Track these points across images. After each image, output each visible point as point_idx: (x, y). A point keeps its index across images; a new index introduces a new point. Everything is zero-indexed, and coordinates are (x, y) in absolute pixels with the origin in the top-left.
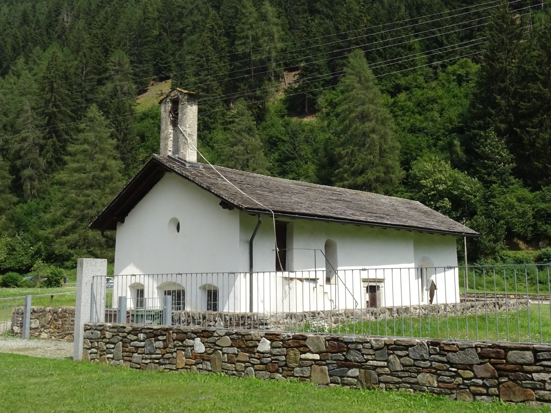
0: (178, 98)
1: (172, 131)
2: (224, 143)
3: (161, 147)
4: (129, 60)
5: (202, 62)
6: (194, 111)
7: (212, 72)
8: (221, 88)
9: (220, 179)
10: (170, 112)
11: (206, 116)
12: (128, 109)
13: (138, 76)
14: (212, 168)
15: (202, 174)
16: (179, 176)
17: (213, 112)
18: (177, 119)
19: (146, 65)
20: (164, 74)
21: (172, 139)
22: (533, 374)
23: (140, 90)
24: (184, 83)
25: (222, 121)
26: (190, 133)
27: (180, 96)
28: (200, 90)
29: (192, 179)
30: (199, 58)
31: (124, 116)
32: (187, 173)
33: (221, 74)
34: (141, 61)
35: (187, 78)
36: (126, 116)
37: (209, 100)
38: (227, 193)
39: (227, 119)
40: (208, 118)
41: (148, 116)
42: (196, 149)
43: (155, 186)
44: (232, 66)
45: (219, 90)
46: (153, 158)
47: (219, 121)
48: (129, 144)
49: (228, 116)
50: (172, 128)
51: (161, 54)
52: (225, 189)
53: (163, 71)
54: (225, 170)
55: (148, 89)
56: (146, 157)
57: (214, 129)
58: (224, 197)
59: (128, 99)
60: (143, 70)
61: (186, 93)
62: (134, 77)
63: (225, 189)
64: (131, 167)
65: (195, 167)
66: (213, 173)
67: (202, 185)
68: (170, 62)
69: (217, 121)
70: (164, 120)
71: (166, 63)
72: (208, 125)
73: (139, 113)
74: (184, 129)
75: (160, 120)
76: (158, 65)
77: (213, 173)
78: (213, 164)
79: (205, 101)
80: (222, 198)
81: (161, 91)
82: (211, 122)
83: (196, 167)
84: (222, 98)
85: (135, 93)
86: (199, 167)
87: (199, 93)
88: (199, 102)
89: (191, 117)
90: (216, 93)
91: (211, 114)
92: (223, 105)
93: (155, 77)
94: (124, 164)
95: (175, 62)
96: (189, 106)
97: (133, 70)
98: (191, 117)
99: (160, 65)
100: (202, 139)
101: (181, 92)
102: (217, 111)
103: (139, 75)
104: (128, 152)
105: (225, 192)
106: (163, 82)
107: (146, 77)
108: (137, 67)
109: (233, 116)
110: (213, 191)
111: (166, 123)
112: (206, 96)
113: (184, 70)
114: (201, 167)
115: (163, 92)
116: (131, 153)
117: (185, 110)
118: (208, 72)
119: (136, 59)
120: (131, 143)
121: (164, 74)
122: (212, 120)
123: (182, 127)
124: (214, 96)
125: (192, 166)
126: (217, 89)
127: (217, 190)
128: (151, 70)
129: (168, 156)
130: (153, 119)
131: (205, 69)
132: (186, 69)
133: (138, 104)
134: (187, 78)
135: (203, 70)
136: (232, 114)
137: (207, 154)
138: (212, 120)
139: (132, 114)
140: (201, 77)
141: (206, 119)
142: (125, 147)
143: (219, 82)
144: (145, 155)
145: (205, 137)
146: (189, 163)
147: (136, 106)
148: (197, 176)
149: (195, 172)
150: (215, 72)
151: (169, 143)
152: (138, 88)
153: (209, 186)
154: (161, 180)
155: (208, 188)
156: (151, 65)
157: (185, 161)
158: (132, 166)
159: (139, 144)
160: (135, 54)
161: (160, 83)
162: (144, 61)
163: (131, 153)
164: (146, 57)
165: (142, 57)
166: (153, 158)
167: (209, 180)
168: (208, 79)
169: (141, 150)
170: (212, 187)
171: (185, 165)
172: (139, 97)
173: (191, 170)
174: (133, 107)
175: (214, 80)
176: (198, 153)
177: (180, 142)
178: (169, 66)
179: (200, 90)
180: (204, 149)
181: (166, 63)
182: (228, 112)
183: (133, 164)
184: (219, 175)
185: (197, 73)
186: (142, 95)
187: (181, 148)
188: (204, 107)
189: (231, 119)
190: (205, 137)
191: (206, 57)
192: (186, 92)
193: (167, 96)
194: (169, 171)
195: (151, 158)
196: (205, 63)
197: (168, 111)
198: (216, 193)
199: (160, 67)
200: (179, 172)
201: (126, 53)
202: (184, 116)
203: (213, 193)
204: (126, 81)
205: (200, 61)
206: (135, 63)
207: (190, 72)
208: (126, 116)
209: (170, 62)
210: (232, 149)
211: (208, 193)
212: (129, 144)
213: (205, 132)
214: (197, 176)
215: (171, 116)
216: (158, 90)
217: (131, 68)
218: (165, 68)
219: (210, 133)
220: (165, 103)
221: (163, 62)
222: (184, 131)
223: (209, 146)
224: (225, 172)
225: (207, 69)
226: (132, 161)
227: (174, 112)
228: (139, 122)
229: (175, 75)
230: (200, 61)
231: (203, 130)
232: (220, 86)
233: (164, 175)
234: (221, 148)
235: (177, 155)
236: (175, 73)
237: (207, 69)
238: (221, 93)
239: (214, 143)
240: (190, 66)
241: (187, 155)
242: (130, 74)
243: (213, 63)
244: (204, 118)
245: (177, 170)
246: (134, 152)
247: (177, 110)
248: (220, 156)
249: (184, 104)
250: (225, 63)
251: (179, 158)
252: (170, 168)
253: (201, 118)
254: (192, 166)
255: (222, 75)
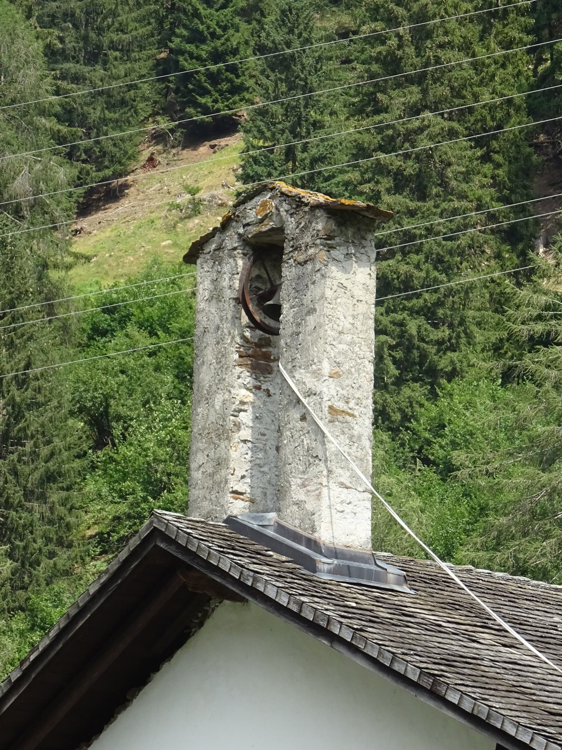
0: (280, 230)
1: (250, 397)
2: (506, 447)
3: (196, 475)
4: (38, 46)
5: (393, 42)
6: (359, 292)
7: (443, 91)
8: (487, 168)
9: (486, 637)
10: (241, 301)
11: (414, 312)
12: (31, 283)
13: (83, 120)
14: (448, 581)
15: (399, 609)
16: (280, 621)
17: (450, 292)
18: (275, 332)
19: (121, 69)
20: (206, 110)
21: (245, 433)
22: (415, 679)
23: (91, 191)
24: (305, 148)
25: (494, 336)
26: (340, 405)
27: (291, 224)
28: (386, 183)
29: (347, 635)
30: (379, 26)
31: (14, 320)
32: (322, 606)
33: (486, 98)
34: (99, 47)
35: (317, 125)
36: (22, 316)
37: (429, 231)
38: (526, 709)
39: (517, 328)
40: (421, 321)
41: (123, 321)
42: (368, 483)
43: (166, 666)
44: (540, 61)
45: (477, 179)
46: (155, 533)
47: (479, 336)
48: (35, 455)
49: (525, 313)
50: (247, 378)
51: (196, 14)
52: (513, 689)
53: (205, 92)
54: (512, 587)
55: (126, 186)
56: (117, 519)
57: (451, 375)
58: (511, 730)
59: (30, 237)
60: (108, 94)
61: (319, 206)
62: (64, 129)
63: (513, 689)
64: (41, 571)
65: (360, 572)
66: (455, 606)
67: (398, 667)
68: (235, 52)
69: (469, 336)
70: (210, 339)
71: (217, 57)
72: (424, 356)
73: (86, 300)
74: (310, 382)
75: (186, 333)
76: (177, 67)
77: (455, 606)
78: (447, 556)
79: (409, 236)
80: (501, 733)
81: (193, 192)
82: (439, 343)
83: (370, 574)
84: (492, 217)
85: (65, 204)
86: (381, 576)
87: (376, 196)
88: (380, 244)
89: (346, 323)
90: (462, 196)
91: (440, 304)
92: (498, 256)
93: (164, 124)
94: (10, 555)
95: (261, 49)
96: (334, 270)
97: (57, 93)
98: (346, 323)
99: (189, 66)
100: (394, 431)
101: (299, 203)
102: (471, 287)
103: (84, 116)
104: (28, 495)
105: (515, 701)
106: (203, 149)
107: (118, 125)
108: (77, 79)
109: (547, 308)
110: (453, 698)
111: (221, 356)
112: (412, 213)
113: (307, 88)
114: (393, 571)
115: (203, 195)
116: (42, 498)
117: (314, 292)
118: (424, 92)
119: (70, 43)
120: (45, 451)
121: (206, 110)
122: (444, 332)
123: (300, 374)
124: (455, 212)
125: (349, 571)
126: (467, 177)
127: (478, 693)
128: (146, 89)
129: (231, 521)
130: (152, 333)
131: (410, 80)
132: (313, 80)
133: (77, 256)
134: (317, 125)
135: (398, 85)
136: (543, 299)
137: (417, 503)
138: (444, 332)
139: (50, 310)
140: (386, 118)
141: (412, 327)
142: (15, 473)
143: (479, 143)
144: (111, 510)
145: (406, 418)
146: (334, 553)
147: (69, 267)
148: (374, 620)
149: (367, 603)
150: (457, 93)
151: (234, 454)
152: (79, 181)
153: (435, 669)
154: (191, 642)
155: (427, 683)
156: (143, 67)
157: (313, 544)
158: (45, 563)
159: (82, 455)
160: (69, 16)
161: (187, 153)
162: (113, 46)
163: (42, 498)
164: (122, 29)
165: (100, 31)
166: (155, 533)
167: (434, 640)
168: (421, 130)
169: (90, 487)
170: (452, 678)
171: (311, 565)
172: (84, 223)
173: (343, 589)
174: (54, 275)
175: (452, 134)
176: (375, 502)
177: (287, 451)
178: (233, 69)
179: (386, 183)
180: (404, 476)
181: (217, 57)
182: (524, 293)
183: (52, 555)
184: (480, 614)
185: (371, 98)
186: (100, 215)
187: (295, 482)
188: (403, 268)
189: (539, 328)
190: (406, 418)
191: (411, 19)
192: (321, 198)
193: (226, 225)
194: (234, 597)
195: (144, 529)
196: (410, 50)
197: (229, 294)
198: (467, 706)
199: (188, 77)
200: (283, 600)
201: (29, 17)
202: (311, 320)
203: (456, 708)
204: (23, 146)
205: (382, 40)
206: (66, 59)
207: (336, 97)
208: (22, 316)
209: (235, 52)
210: (545, 477)
211: (432, 704)
212: (35, 455)
213: (406, 391)
214: (374, 620)
215: (245, 319)
216: (175, 187)
217: (47, 84)
218: (214, 78)
219: (433, 396)
220: (217, 260)
221: (204, 50)
222: (310, 394)
223: (426, 461)
224: (512, 598)
225: (420, 79)
226: (48, 540)
227: (262, 299)
228: (83, 347)
229: (263, 113)
230: (382, 40)
231: (399, 382)
232: (486, 158)
233: (206, 615)
234: (489, 474)
235: (272, 515)
236: (260, 103)
237: (420, 79)
238: (487, 194)
239: (454, 445)
240: (333, 65)
241: (325, 512)
242: (43, 112)
243: (450, 45)
244: (401, 324)
245: (271, 593)
246: (55, 496)
247: (274, 290)
248: (483, 510)
249: (311, 259)
250: (508, 44)
251: (281, 529)
252: (239, 583)
253: (385, 320)
254: (349, 571)
255: (492, 108)
